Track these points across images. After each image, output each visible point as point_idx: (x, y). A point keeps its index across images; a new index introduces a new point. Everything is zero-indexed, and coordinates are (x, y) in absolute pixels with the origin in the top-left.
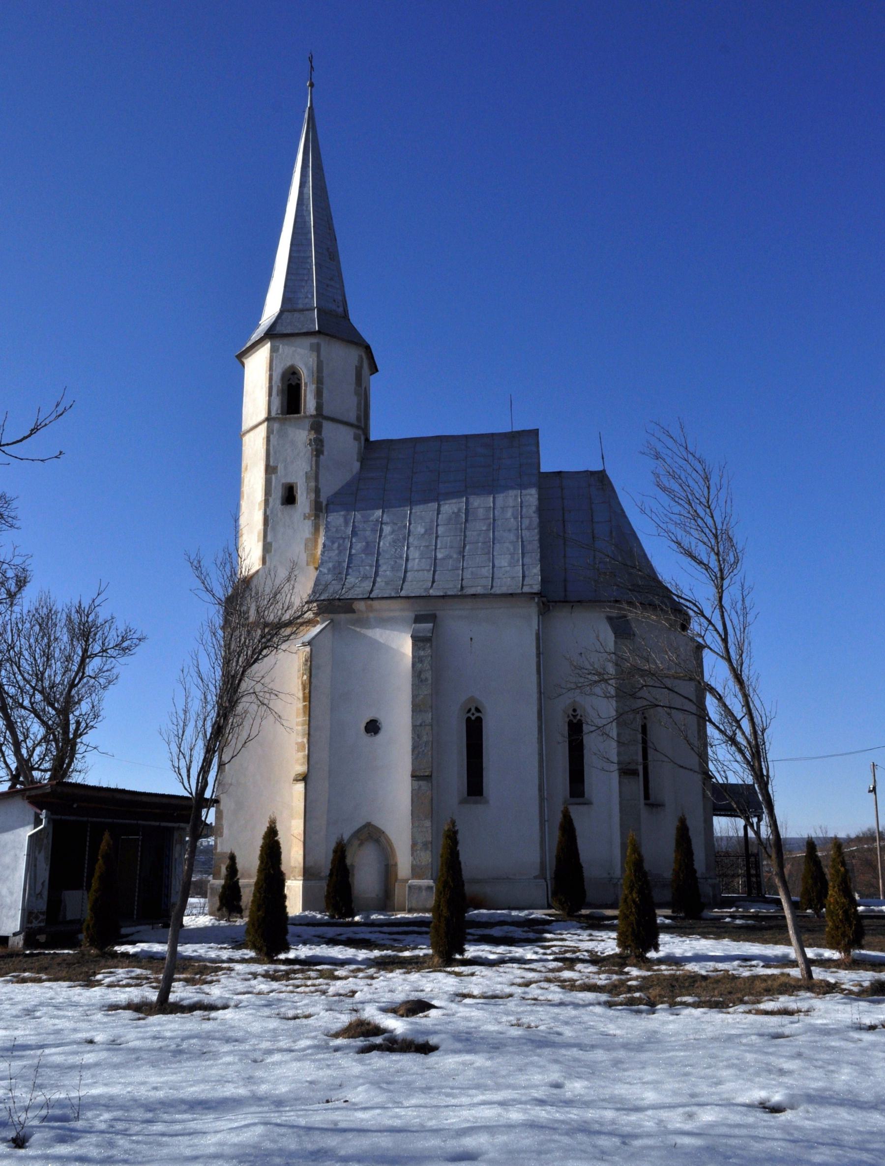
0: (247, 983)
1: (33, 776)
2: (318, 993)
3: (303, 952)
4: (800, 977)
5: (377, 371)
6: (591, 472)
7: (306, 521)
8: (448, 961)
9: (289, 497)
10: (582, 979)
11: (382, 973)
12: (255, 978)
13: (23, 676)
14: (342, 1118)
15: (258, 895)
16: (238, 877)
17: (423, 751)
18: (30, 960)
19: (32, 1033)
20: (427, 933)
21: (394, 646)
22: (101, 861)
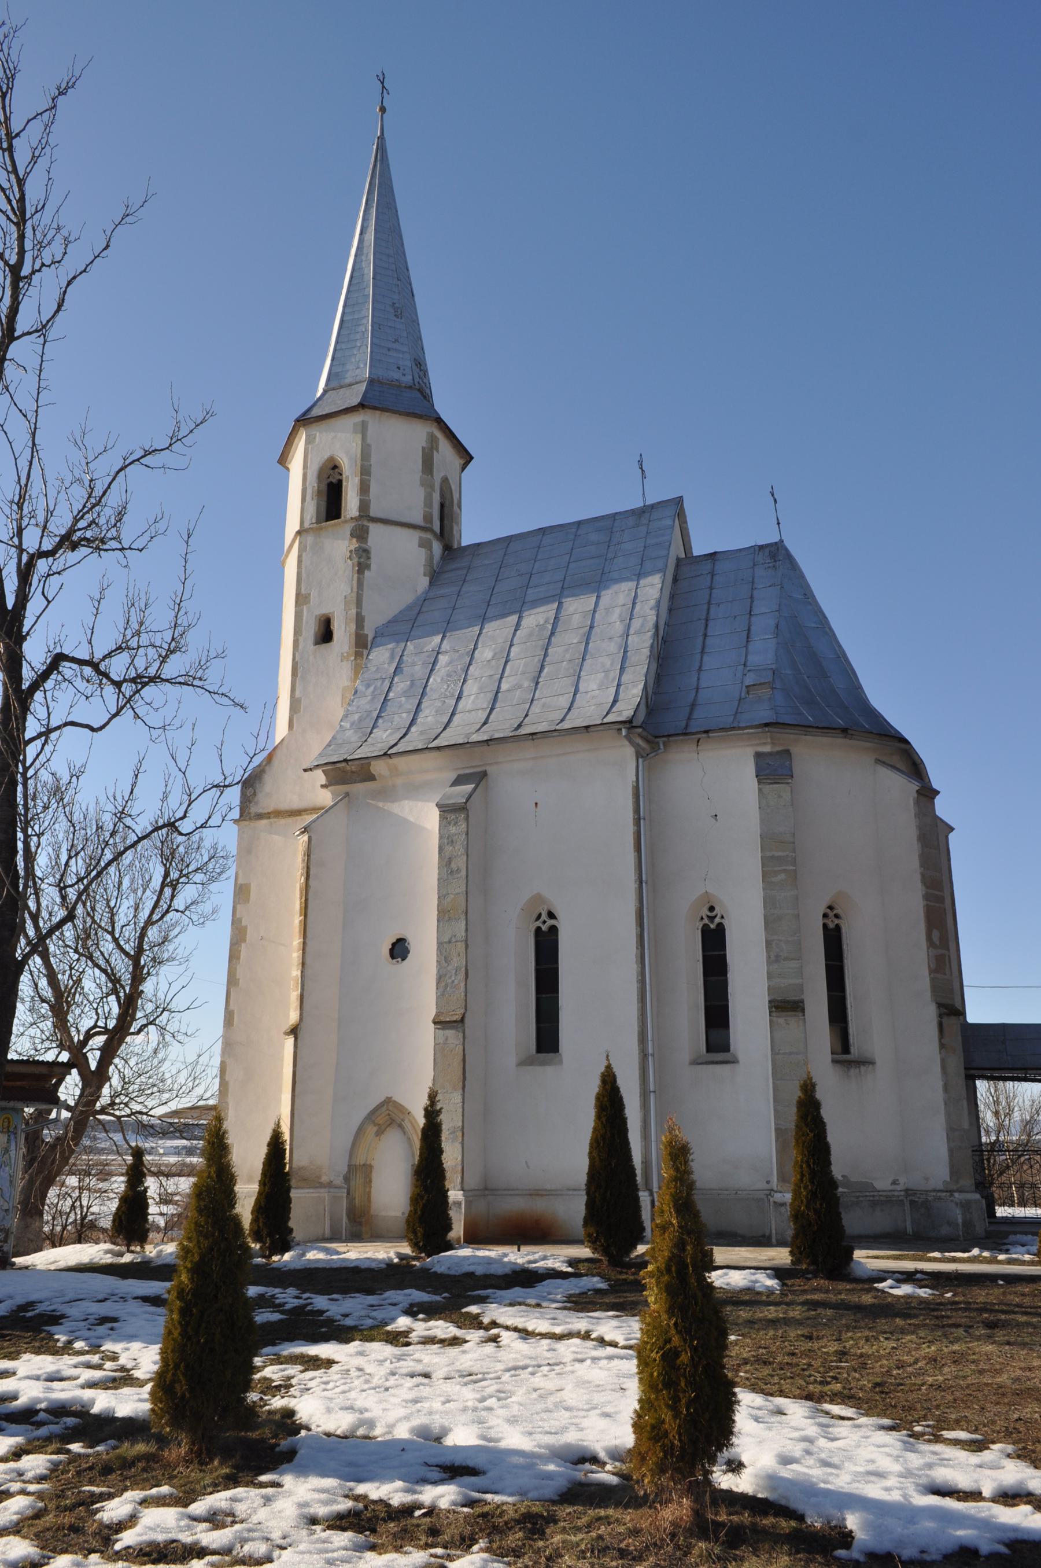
5: (472, 458)
6: (759, 546)
7: (345, 663)
9: (325, 635)
17: (453, 981)
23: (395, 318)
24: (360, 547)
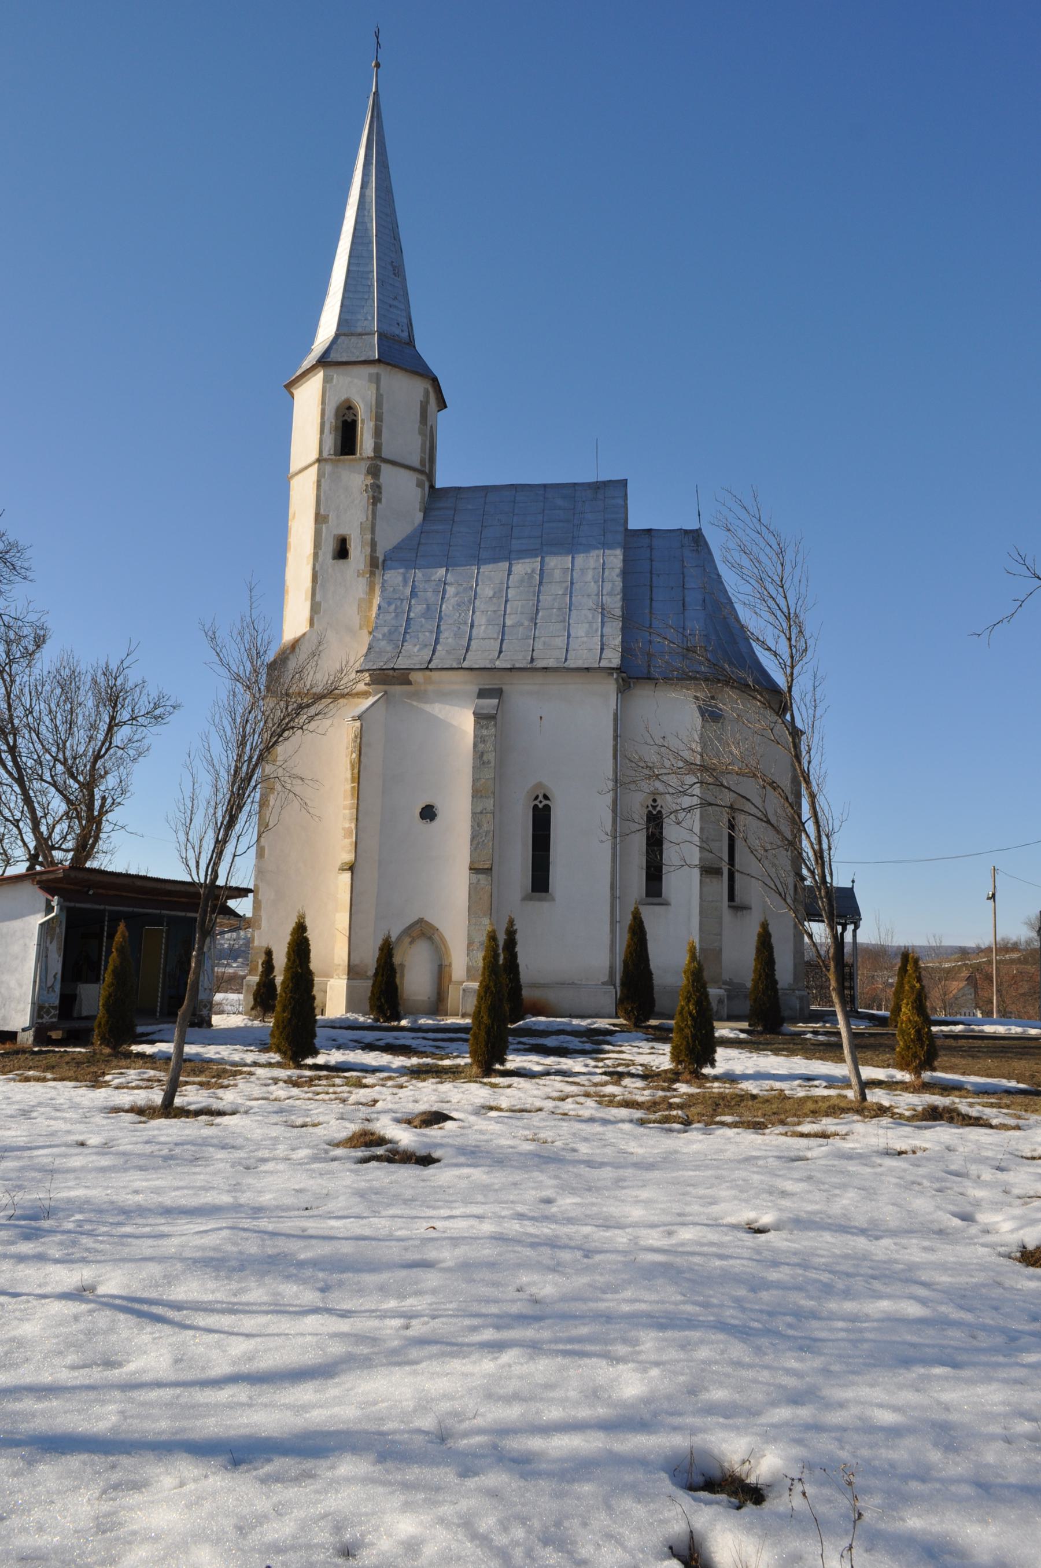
0: (265, 1089)
1: (52, 857)
2: (338, 1101)
3: (335, 1057)
4: (854, 1099)
5: (446, 407)
7: (360, 579)
8: (488, 1072)
9: (342, 552)
10: (623, 1095)
11: (414, 1082)
12: (276, 1084)
13: (42, 745)
14: (313, 1226)
15: (284, 995)
16: (274, 974)
18: (37, 1058)
19: (24, 1134)
20: (466, 1040)
21: (455, 723)
22: (115, 954)
23: (393, 276)
24: (374, 483)
